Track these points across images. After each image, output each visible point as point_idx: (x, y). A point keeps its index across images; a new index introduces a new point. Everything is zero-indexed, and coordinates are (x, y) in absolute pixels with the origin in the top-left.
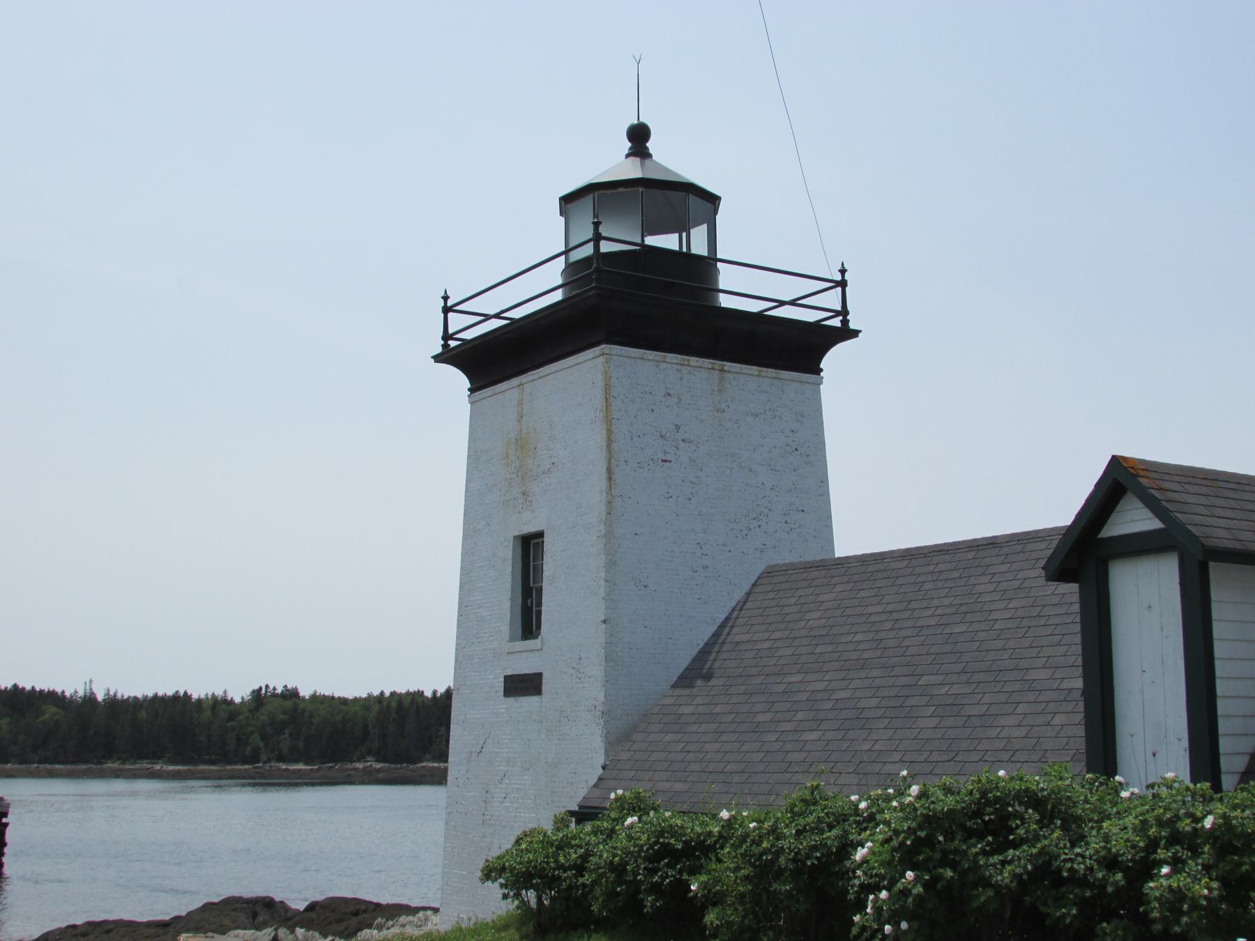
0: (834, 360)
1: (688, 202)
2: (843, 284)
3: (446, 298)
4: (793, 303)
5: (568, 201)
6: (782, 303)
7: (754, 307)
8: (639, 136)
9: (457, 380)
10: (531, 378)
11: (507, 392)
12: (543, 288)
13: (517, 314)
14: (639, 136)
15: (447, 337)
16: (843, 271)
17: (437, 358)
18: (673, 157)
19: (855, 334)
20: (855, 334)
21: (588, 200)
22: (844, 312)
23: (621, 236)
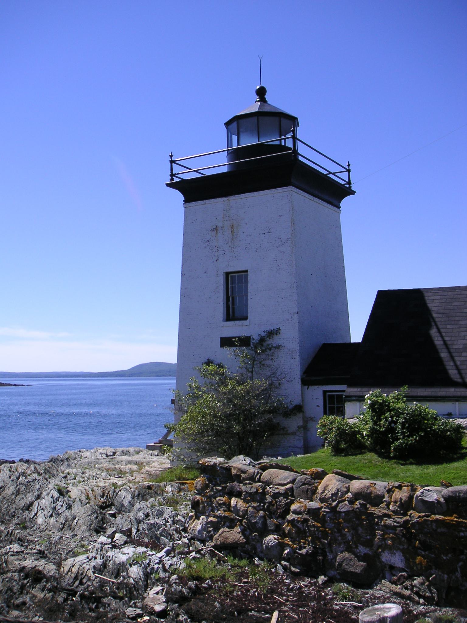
0: (346, 202)
1: (286, 122)
2: (349, 171)
3: (171, 156)
4: (334, 174)
5: (227, 124)
6: (330, 173)
7: (325, 172)
8: (261, 92)
9: (178, 196)
10: (281, 191)
11: (198, 206)
12: (218, 164)
13: (208, 173)
14: (261, 92)
15: (172, 175)
16: (349, 165)
17: (168, 185)
18: (277, 101)
19: (353, 193)
20: (353, 193)
21: (235, 124)
22: (349, 183)
23: (249, 141)
